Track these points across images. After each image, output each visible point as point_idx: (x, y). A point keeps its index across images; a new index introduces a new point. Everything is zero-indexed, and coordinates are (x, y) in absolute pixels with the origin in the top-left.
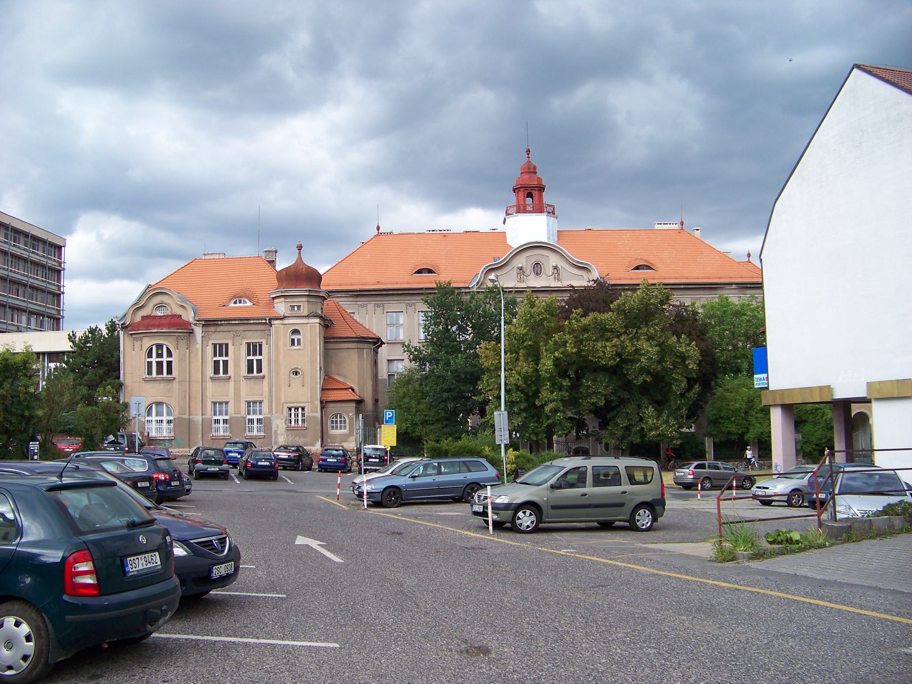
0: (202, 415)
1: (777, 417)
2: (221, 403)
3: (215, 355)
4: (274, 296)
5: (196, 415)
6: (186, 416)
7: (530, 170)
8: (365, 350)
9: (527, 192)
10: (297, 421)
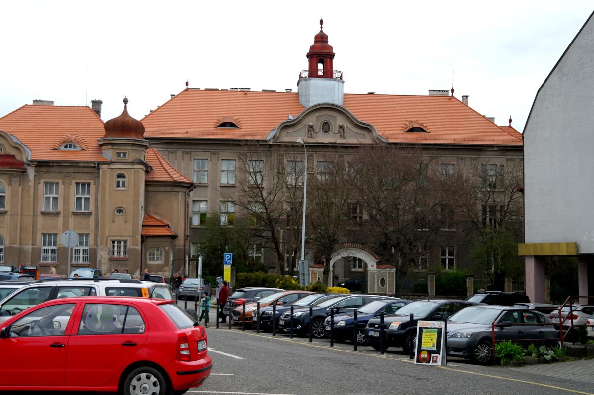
0: (33, 245)
1: (530, 267)
2: (50, 235)
3: (77, 193)
4: (102, 143)
5: (26, 244)
6: (17, 246)
7: (321, 38)
8: (180, 193)
9: (319, 58)
10: (119, 252)
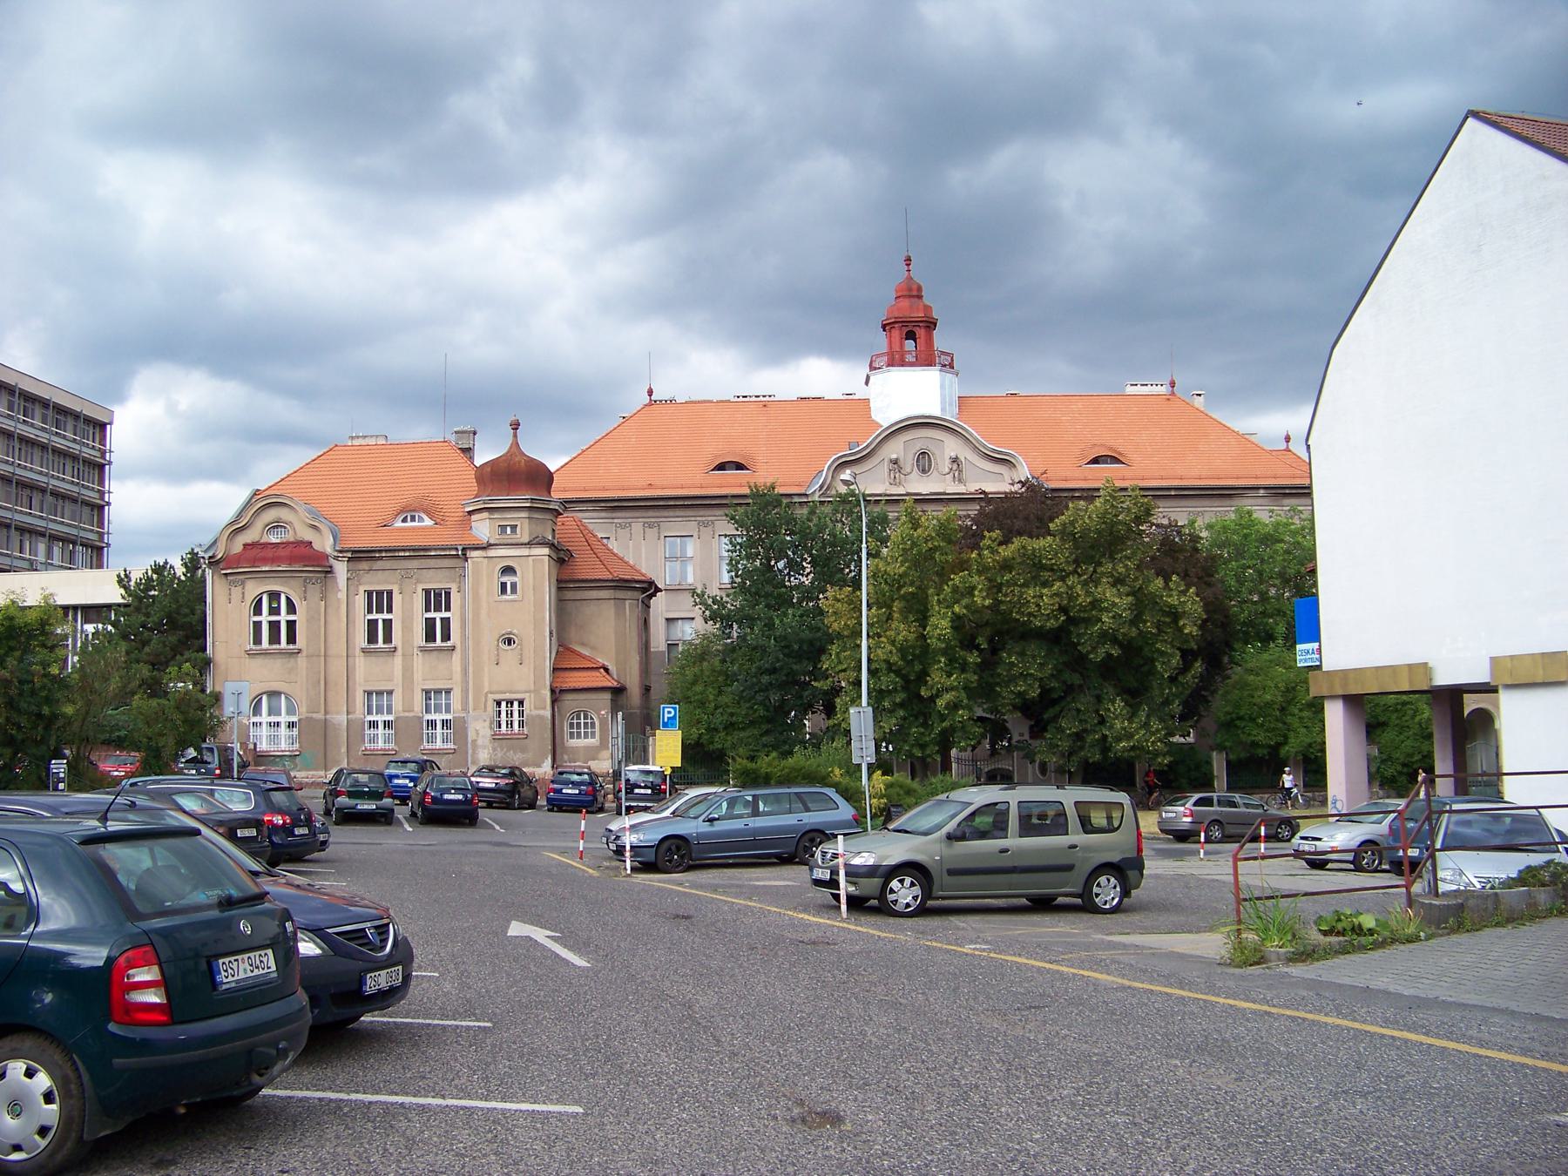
0: (348, 713)
1: (1335, 717)
2: (379, 693)
3: (370, 611)
4: (471, 509)
5: (338, 713)
6: (320, 716)
7: (912, 292)
8: (627, 602)
9: (905, 330)
10: (510, 724)
